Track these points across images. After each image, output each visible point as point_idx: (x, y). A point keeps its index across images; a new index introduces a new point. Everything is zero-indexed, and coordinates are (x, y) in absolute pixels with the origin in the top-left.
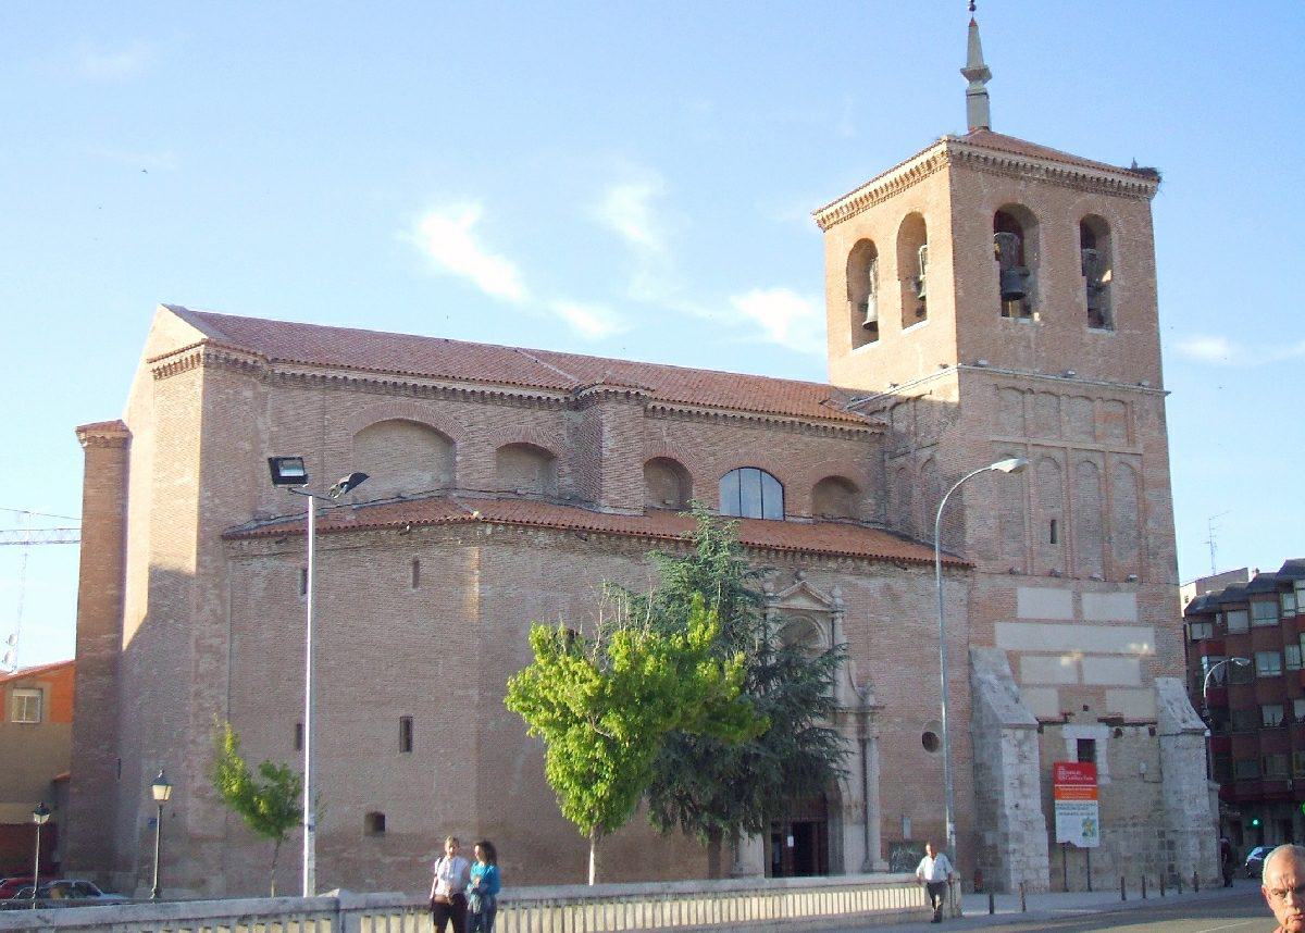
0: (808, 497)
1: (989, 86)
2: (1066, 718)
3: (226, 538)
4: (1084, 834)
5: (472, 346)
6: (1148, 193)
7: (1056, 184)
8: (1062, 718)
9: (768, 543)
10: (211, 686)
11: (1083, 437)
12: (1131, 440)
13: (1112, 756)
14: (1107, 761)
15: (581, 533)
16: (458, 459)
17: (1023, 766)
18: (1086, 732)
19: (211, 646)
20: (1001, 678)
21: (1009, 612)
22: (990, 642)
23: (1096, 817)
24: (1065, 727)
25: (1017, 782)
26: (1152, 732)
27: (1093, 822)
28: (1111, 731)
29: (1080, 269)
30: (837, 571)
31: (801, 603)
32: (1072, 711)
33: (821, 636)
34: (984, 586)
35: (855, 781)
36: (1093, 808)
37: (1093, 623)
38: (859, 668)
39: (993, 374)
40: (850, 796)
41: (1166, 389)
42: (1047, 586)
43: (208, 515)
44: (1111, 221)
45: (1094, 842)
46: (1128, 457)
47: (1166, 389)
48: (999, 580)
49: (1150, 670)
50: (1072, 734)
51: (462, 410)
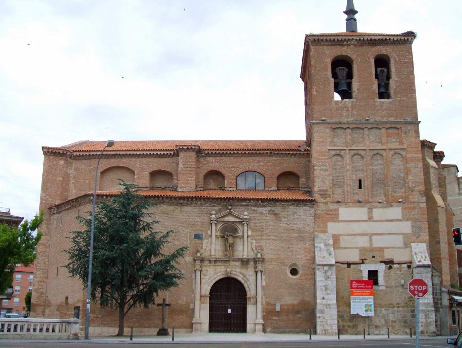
0: (275, 180)
1: (356, 16)
2: (363, 262)
3: (50, 208)
4: (366, 311)
5: (166, 141)
6: (411, 42)
7: (362, 45)
8: (361, 262)
9: (274, 197)
10: (42, 256)
11: (377, 144)
12: (401, 143)
13: (386, 276)
14: (384, 279)
15: (176, 198)
16: (135, 177)
17: (327, 282)
18: (373, 268)
19: (43, 243)
20: (326, 245)
21: (335, 218)
22: (324, 231)
23: (372, 303)
24: (362, 265)
25: (324, 288)
26: (409, 267)
27: (370, 306)
28: (386, 267)
29: (374, 76)
30: (247, 206)
31: (230, 218)
32: (367, 258)
33: (239, 231)
34: (322, 208)
35: (252, 287)
36: (371, 300)
37: (344, 221)
38: (256, 243)
39: (329, 123)
40: (250, 294)
41: (419, 120)
42: (355, 207)
43: (44, 201)
44: (389, 55)
45: (371, 314)
46: (398, 151)
47: (419, 120)
48: (330, 206)
49: (409, 240)
50: (365, 269)
51: (139, 161)
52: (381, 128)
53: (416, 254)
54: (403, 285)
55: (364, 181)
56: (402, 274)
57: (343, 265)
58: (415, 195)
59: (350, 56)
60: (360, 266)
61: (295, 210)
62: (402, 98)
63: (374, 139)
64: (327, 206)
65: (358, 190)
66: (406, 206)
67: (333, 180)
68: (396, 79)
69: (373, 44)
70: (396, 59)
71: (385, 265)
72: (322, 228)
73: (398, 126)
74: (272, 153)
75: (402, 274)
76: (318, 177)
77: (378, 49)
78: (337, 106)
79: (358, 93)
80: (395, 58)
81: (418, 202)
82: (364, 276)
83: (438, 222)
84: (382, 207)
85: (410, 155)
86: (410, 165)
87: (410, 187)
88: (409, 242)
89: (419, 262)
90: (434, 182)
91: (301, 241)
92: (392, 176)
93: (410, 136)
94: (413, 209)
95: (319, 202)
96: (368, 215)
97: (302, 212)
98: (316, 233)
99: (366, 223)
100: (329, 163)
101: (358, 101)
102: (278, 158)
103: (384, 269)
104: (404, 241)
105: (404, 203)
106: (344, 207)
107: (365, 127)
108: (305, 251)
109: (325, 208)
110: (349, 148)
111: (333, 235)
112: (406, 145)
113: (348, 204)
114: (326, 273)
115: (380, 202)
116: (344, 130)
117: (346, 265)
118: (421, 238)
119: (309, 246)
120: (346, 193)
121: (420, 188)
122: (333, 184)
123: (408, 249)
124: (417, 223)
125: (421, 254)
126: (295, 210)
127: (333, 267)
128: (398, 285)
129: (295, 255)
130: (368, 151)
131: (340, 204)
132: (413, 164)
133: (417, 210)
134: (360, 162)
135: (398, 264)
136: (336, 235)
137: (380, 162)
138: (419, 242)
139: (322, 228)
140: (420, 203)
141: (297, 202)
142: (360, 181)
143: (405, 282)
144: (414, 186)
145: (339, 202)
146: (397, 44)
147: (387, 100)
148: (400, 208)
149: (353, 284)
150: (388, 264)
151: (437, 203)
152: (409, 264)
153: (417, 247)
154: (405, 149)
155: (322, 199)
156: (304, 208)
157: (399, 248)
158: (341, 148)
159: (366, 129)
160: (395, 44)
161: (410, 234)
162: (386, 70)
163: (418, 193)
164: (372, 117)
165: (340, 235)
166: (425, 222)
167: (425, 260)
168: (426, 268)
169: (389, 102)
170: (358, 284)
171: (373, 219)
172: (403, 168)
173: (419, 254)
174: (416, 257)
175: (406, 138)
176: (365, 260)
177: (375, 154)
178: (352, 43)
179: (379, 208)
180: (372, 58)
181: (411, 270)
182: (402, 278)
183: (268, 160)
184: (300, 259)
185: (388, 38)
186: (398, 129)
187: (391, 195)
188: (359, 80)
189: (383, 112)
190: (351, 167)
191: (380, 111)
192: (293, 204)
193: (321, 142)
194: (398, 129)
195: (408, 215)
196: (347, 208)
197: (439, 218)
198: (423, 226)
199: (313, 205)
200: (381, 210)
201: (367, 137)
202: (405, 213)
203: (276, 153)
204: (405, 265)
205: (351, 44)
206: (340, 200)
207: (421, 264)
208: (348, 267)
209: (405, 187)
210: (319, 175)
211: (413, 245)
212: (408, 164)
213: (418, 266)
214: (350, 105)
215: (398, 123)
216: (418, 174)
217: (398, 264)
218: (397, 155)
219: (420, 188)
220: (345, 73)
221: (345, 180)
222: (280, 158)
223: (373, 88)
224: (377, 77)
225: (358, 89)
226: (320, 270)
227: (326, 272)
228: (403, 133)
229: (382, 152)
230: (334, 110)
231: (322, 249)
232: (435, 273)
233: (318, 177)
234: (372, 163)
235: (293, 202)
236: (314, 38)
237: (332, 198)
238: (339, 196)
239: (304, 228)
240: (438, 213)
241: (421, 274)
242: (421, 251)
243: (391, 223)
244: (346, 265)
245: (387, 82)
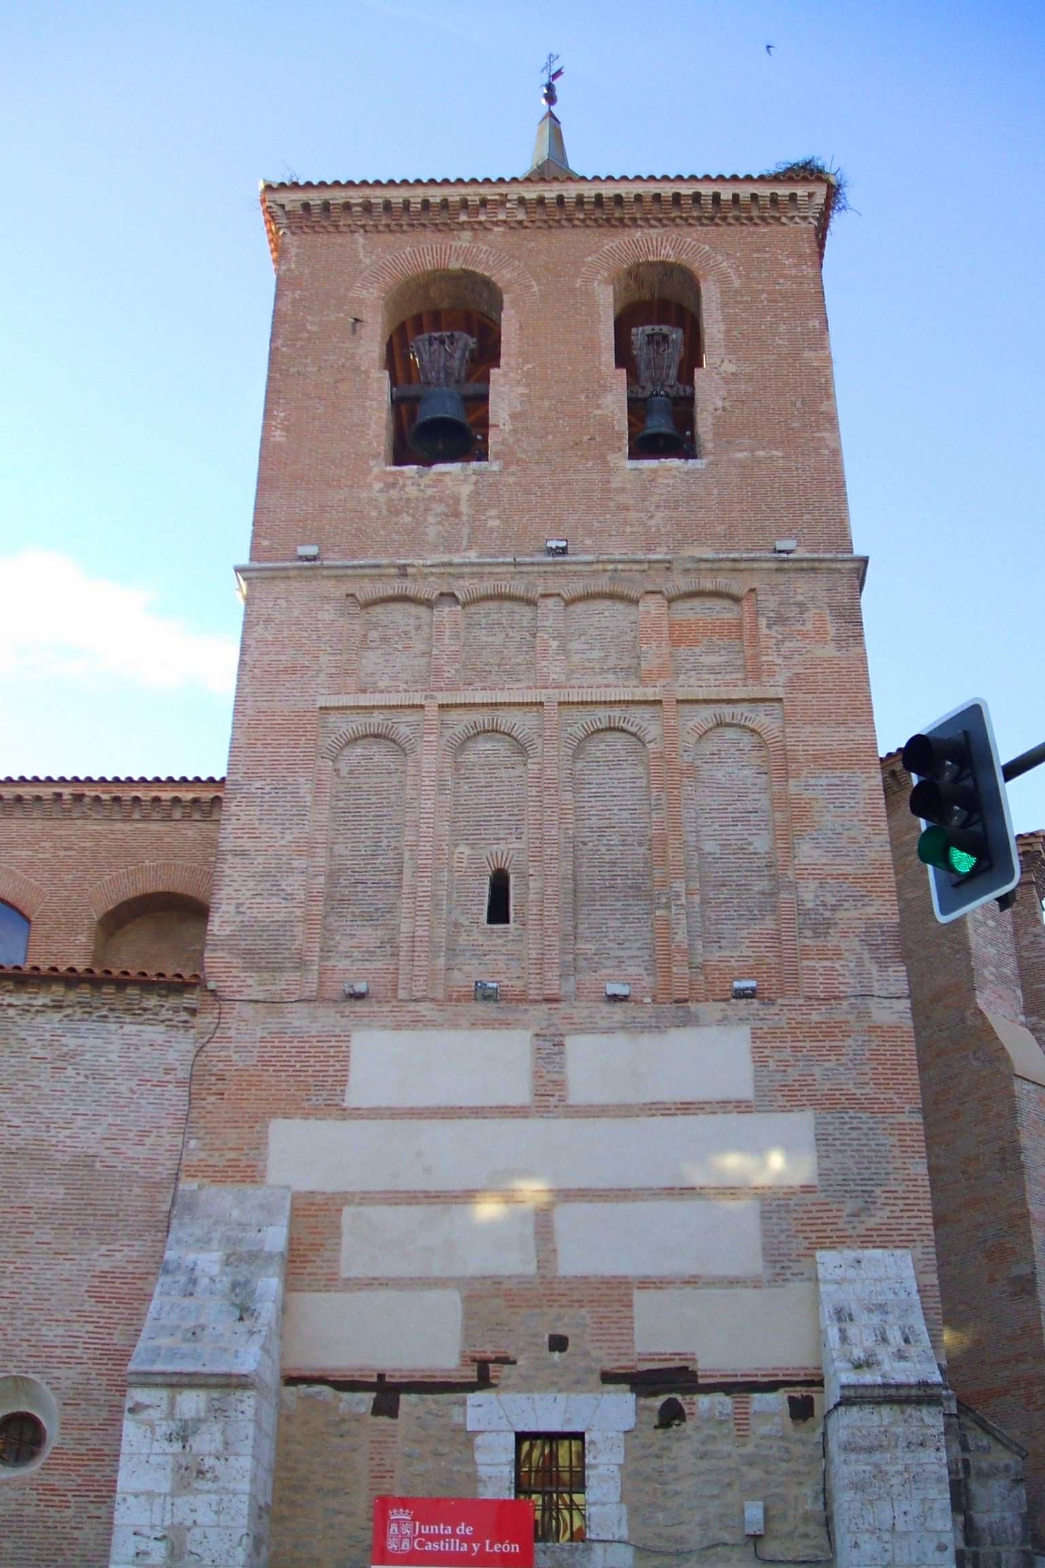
0: (82, 939)
8: (471, 1374)
11: (611, 678)
12: (755, 672)
24: (473, 1398)
26: (801, 1410)
28: (639, 1410)
29: (609, 357)
32: (511, 1353)
41: (858, 551)
42: (456, 1026)
44: (695, 266)
46: (739, 709)
48: (299, 1018)
52: (633, 594)
53: (842, 1315)
54: (756, 1538)
55: (524, 876)
56: (750, 1462)
57: (346, 1396)
58: (838, 954)
59: (487, 274)
60: (464, 1403)
61: (71, 1042)
62: (761, 453)
63: (596, 654)
64: (274, 1024)
65: (484, 933)
66: (777, 1016)
67: (333, 876)
68: (730, 368)
69: (608, 220)
70: (731, 282)
71: (631, 1397)
72: (233, 1155)
73: (737, 586)
74: (86, 800)
75: (750, 1462)
76: (243, 854)
77: (636, 244)
78: (394, 493)
79: (515, 431)
80: (724, 280)
81: (859, 991)
82: (483, 1471)
83: (1021, 1167)
84: (625, 1027)
85: (808, 728)
86: (808, 786)
87: (810, 905)
88: (800, 1244)
89: (858, 1366)
90: (991, 951)
91: (82, 1231)
92: (699, 849)
93: (805, 635)
94: (827, 1034)
95: (227, 995)
96: (537, 1075)
97: (114, 1057)
98: (188, 1185)
99: (518, 1124)
100: (319, 783)
101: (513, 468)
102: (119, 826)
103: (630, 1422)
104: (766, 1233)
105: (772, 1002)
106: (385, 1027)
107: (540, 590)
108: (100, 1300)
109: (260, 1033)
110: (444, 698)
111: (296, 1196)
112: (781, 679)
113: (412, 1006)
114: (184, 1439)
115: (614, 998)
116: (422, 611)
117: (368, 1398)
118: (879, 1217)
119: (130, 1268)
120: (405, 947)
121: (870, 910)
122: (329, 897)
123: (798, 1288)
124: (855, 1123)
125: (876, 1319)
126: (71, 1042)
127: (239, 1394)
128: (726, 1537)
129: (32, 1322)
130: (552, 712)
131: (360, 1007)
132: (824, 782)
133: (849, 1041)
134: (503, 773)
135: (728, 1388)
136: (319, 1199)
137: (628, 773)
138: (866, 1241)
139: (233, 1155)
140: (872, 1003)
141: (85, 991)
142: (500, 886)
143: (767, 1519)
144: (831, 900)
145: (359, 997)
146: (737, 218)
147: (674, 463)
148: (745, 1031)
149: (393, 1528)
150: (655, 1394)
151: (1007, 1059)
152: (799, 1392)
153: (851, 1273)
154: (780, 700)
155: (250, 981)
156: (128, 1029)
157: (734, 1282)
158: (394, 699)
159: (550, 602)
160: (724, 219)
161: (807, 1189)
162: (676, 335)
163: (855, 943)
164: (588, 542)
165: (346, 1198)
166: (902, 1118)
167: (901, 1356)
168: (909, 1410)
169: (687, 473)
170: (425, 1530)
171: (562, 1099)
172: (764, 802)
173: (864, 1318)
174: (844, 1338)
175: (779, 643)
176: (504, 1361)
177: (598, 731)
178: (502, 217)
179: (609, 1031)
180: (607, 282)
181: (817, 1436)
182: (752, 1490)
183: (60, 837)
184: (58, 1352)
185: (686, 190)
186: (736, 599)
187: (689, 951)
188: (528, 374)
189: (651, 517)
190: (448, 799)
191: (632, 515)
192: (58, 1006)
193: (285, 671)
194: (736, 599)
195: (793, 1073)
196: (406, 1036)
197: (1024, 1141)
198: (893, 1140)
199: (193, 1012)
200: (619, 1044)
201: (554, 644)
202: (772, 1065)
203: (104, 797)
204: (777, 1401)
205: (496, 224)
206: (361, 987)
207: (868, 1377)
208: (377, 1410)
209: (775, 909)
210: (248, 844)
211: (829, 1261)
212: (792, 782)
213: (853, 1398)
214: (466, 490)
215: (736, 567)
216: (852, 833)
217: (728, 1388)
218: (730, 734)
219: (870, 910)
220: (458, 355)
221: (407, 872)
222: (127, 827)
223: (598, 407)
224: (624, 357)
225: (514, 417)
226: (145, 1415)
227: (183, 1434)
228: (763, 622)
229: (639, 718)
230: (374, 514)
231: (204, 1281)
232: (987, 1450)
233: (243, 854)
234: (577, 783)
235: (58, 990)
236: (302, 196)
237: (314, 976)
238: (358, 965)
239: (116, 1152)
240: (1014, 1112)
241: (871, 1450)
242: (881, 1300)
243: (681, 1121)
244: (368, 1398)
245: (682, 390)
